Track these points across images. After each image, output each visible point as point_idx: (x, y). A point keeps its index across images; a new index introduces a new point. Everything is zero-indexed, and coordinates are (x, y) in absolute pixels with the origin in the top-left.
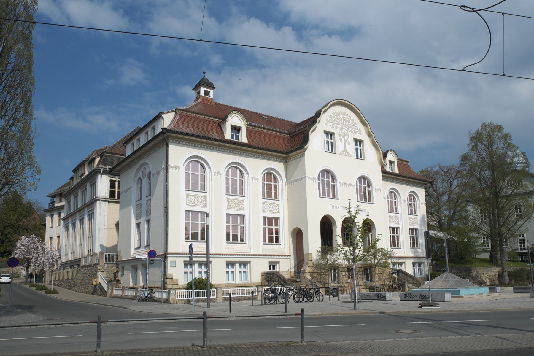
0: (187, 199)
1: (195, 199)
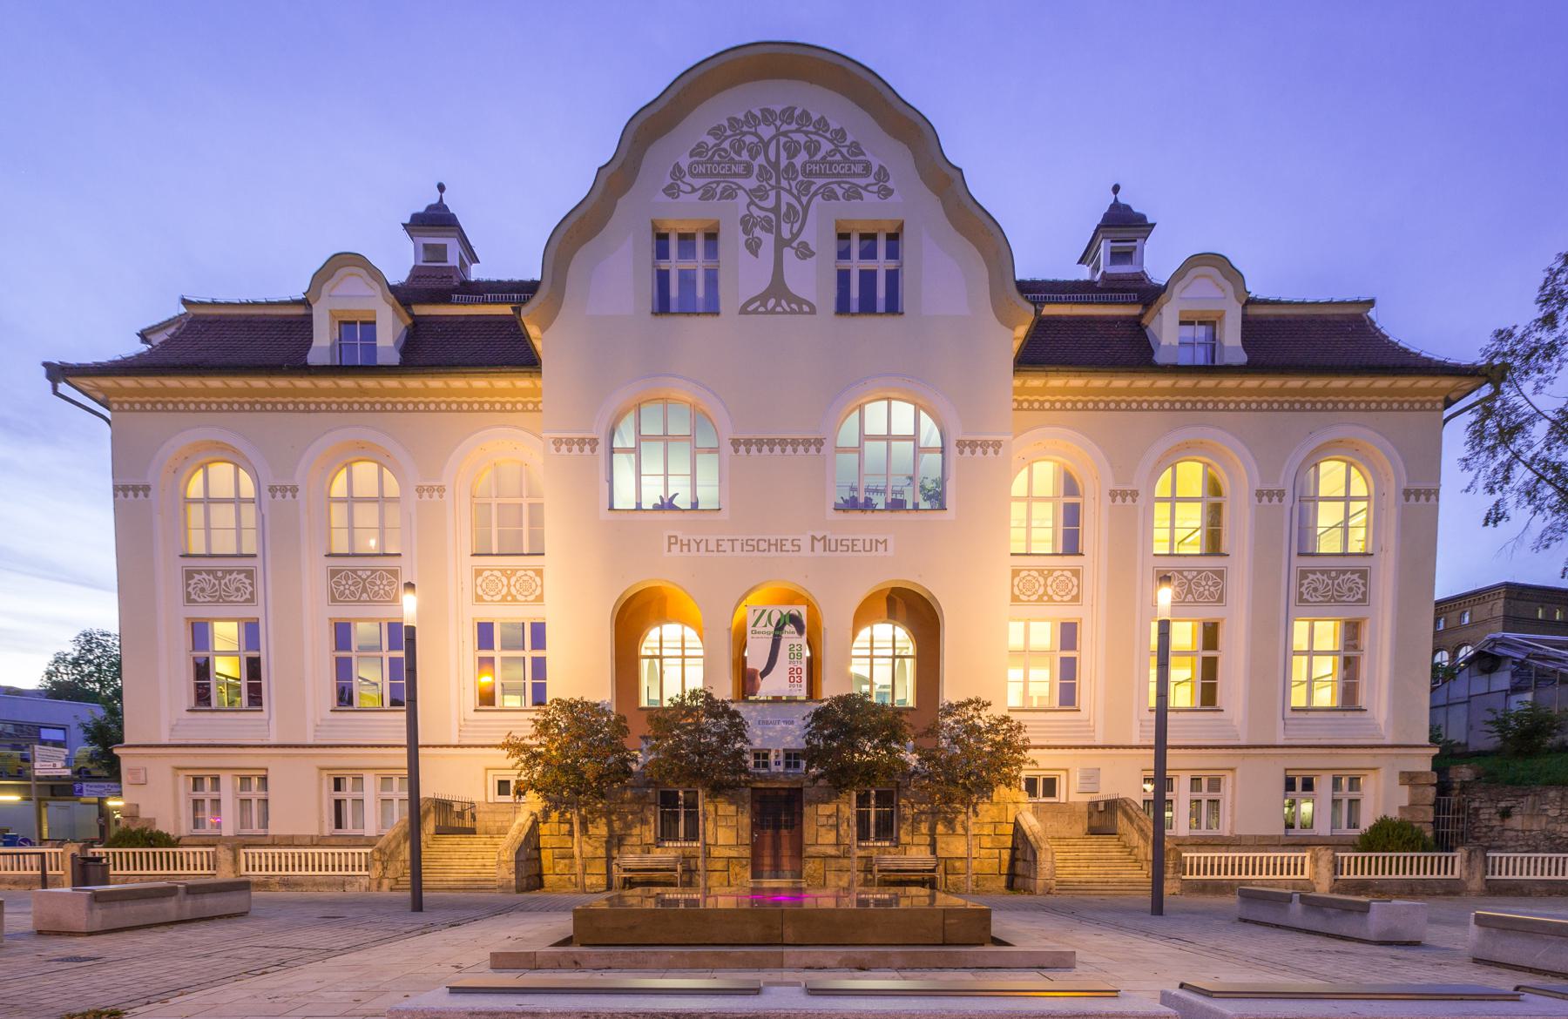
0: (188, 585)
1: (217, 582)
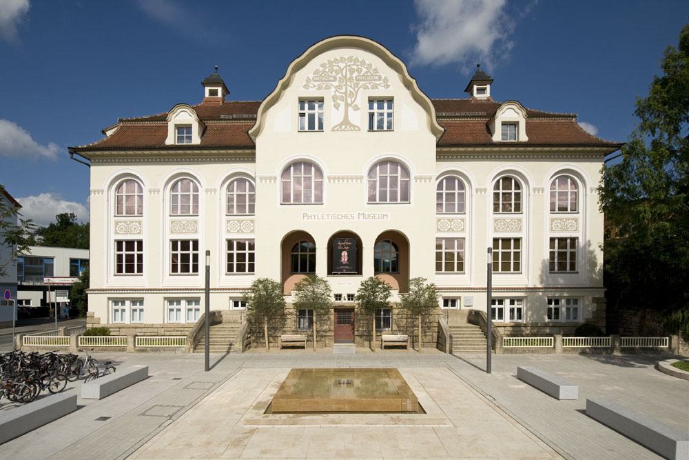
0: (552, 224)
